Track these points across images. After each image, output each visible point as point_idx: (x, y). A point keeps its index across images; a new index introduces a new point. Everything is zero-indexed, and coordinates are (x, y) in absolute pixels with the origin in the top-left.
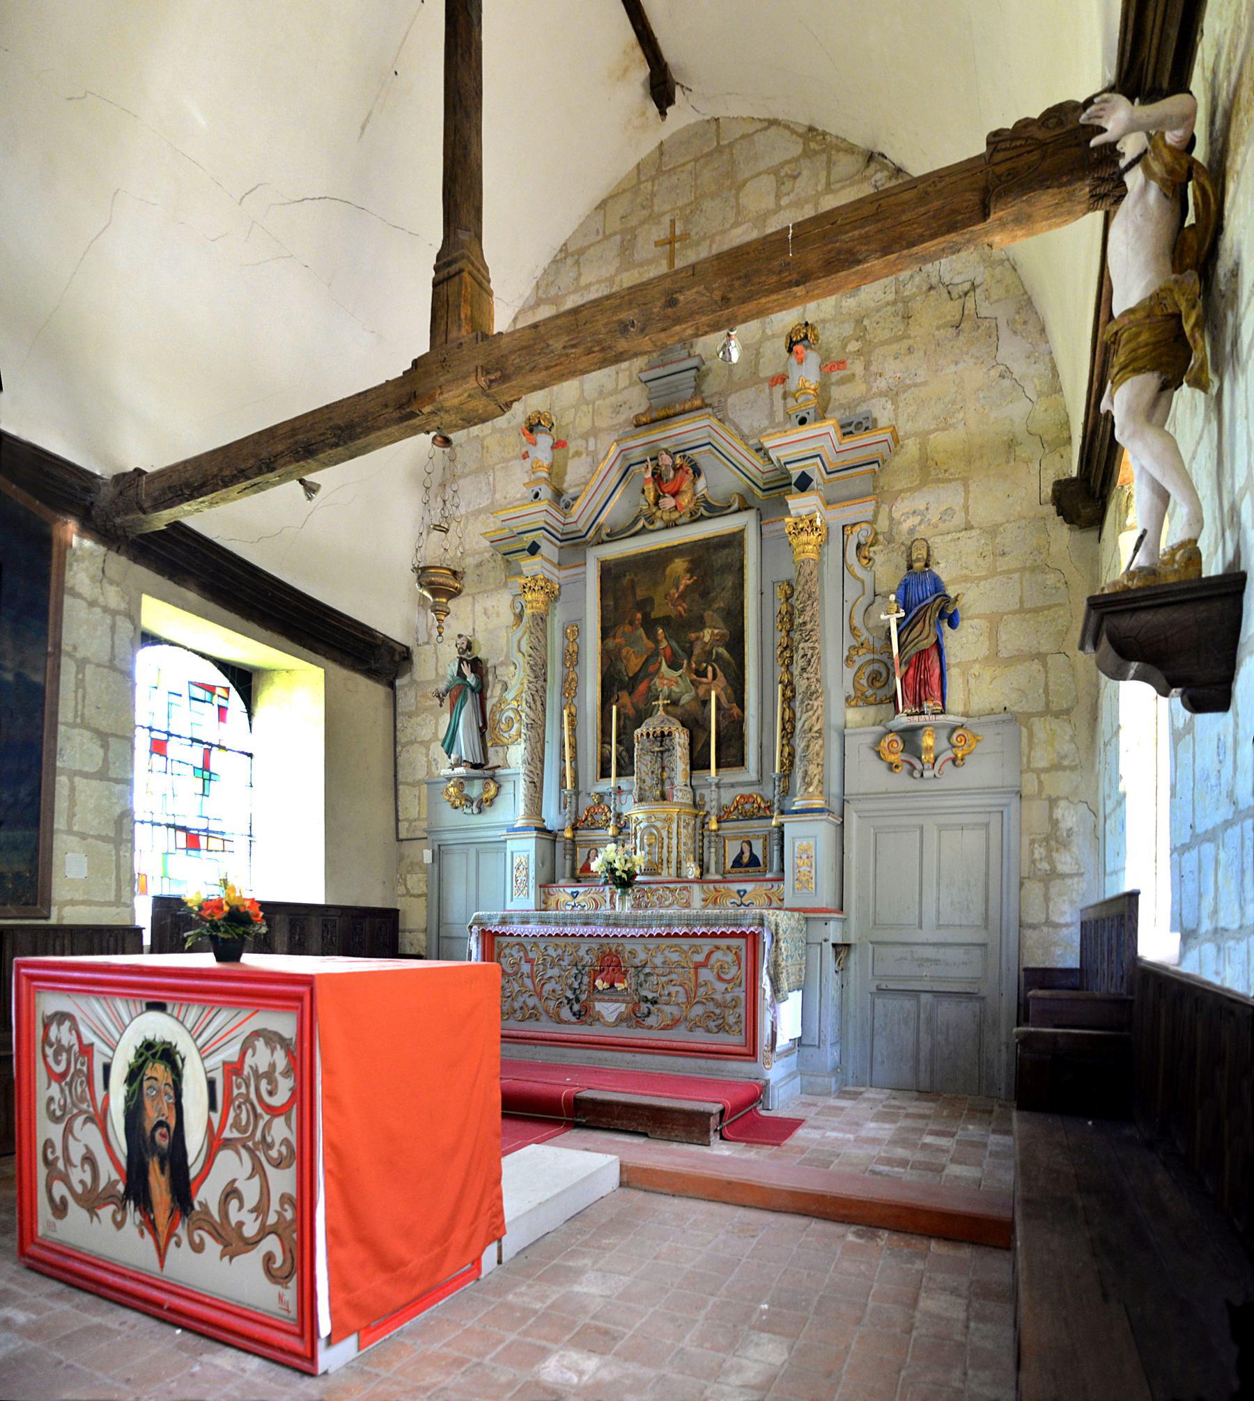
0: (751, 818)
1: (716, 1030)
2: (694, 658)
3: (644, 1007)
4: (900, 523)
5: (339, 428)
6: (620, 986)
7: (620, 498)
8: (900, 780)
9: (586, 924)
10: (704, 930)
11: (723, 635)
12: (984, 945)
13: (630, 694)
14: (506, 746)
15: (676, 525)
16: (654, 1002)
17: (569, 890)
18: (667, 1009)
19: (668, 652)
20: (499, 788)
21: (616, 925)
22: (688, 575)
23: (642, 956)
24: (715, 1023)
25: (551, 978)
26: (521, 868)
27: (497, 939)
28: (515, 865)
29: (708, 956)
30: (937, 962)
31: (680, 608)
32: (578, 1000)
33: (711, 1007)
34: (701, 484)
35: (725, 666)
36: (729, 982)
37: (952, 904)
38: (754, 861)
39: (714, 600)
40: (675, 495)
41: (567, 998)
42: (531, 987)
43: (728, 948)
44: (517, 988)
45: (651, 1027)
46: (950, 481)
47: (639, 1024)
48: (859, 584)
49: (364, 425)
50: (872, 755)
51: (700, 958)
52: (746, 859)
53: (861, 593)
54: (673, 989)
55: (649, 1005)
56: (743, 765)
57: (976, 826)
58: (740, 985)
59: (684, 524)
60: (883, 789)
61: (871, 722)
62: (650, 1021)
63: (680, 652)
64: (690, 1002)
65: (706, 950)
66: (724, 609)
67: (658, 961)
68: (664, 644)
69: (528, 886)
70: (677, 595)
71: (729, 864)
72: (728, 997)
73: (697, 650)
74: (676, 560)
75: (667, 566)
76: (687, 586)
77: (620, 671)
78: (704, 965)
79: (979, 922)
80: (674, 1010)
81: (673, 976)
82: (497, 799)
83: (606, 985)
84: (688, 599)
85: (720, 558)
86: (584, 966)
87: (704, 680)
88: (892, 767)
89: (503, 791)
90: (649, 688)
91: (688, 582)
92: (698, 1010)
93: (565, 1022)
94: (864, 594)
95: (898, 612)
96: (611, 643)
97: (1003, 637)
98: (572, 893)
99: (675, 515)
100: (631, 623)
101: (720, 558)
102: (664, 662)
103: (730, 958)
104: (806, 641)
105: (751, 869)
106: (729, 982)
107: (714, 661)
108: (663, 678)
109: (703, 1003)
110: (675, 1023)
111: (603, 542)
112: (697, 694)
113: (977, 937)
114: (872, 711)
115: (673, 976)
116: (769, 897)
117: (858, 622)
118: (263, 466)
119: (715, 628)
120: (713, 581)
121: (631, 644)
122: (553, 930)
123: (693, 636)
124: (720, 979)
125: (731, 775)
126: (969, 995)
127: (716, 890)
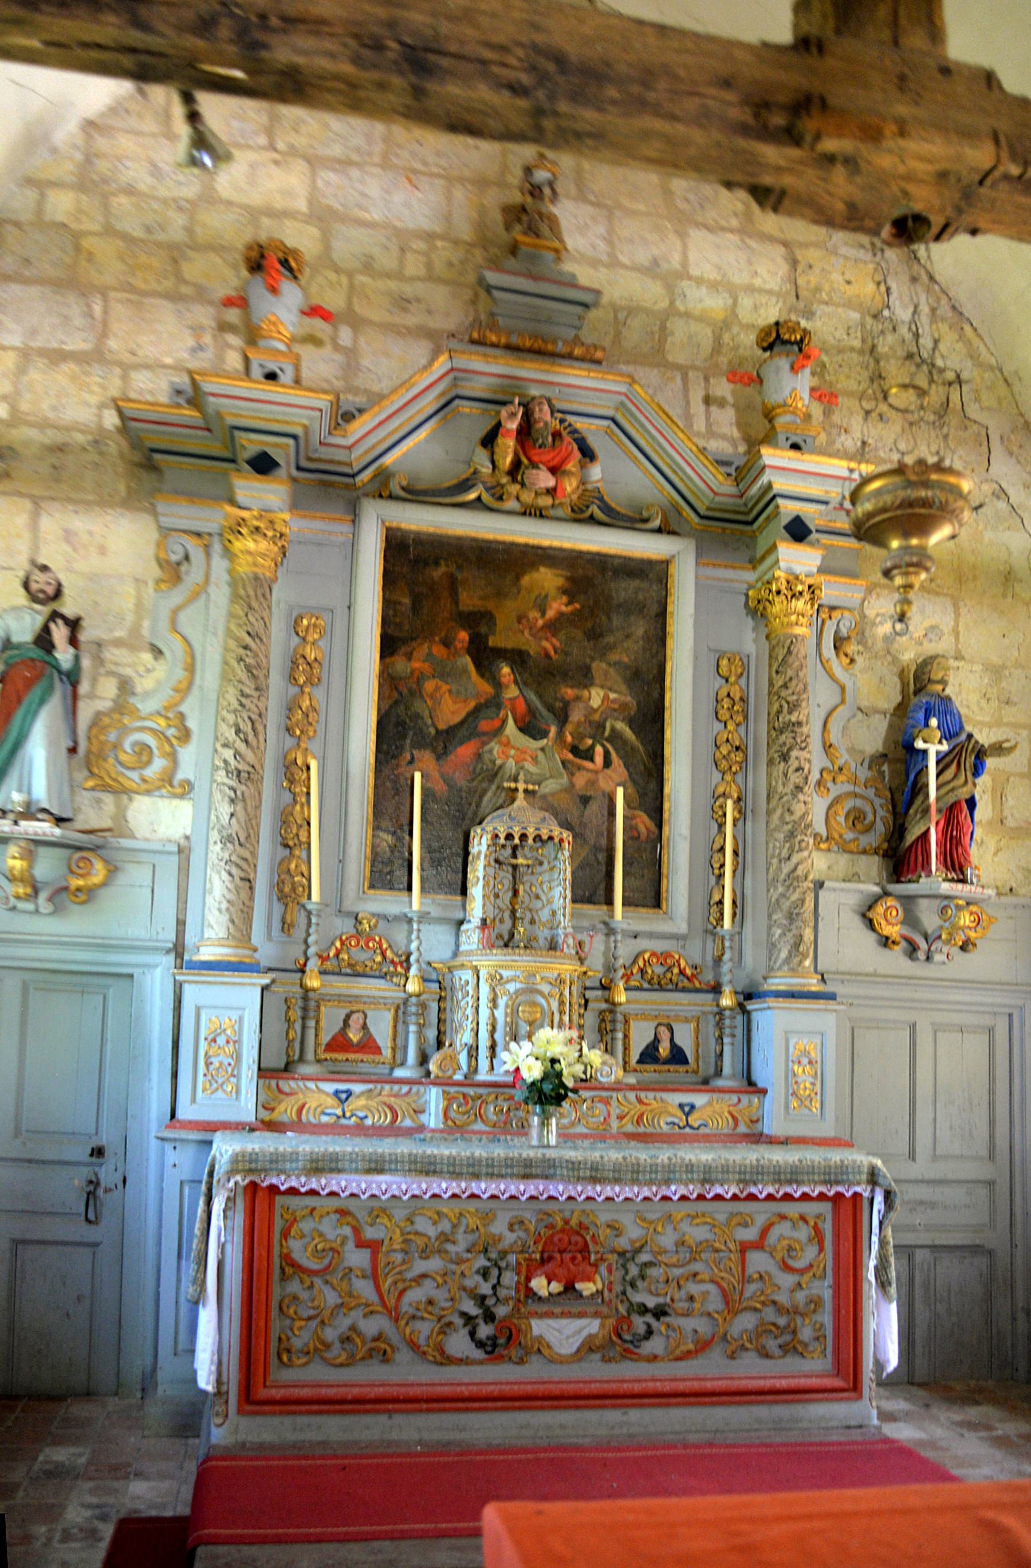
0: (661, 988)
1: (778, 1352)
2: (569, 728)
3: (639, 1323)
4: (874, 624)
5: (560, 60)
6: (587, 1288)
7: (427, 440)
8: (895, 960)
9: (526, 1177)
10: (770, 1189)
11: (624, 706)
12: (991, 1184)
13: (438, 758)
14: (121, 791)
15: (541, 516)
16: (660, 1313)
17: (330, 1087)
18: (687, 1324)
19: (522, 707)
20: (113, 870)
21: (594, 1180)
22: (565, 599)
23: (633, 1232)
24: (781, 1341)
25: (424, 1276)
26: (221, 1040)
27: (279, 1200)
28: (203, 1034)
29: (765, 1232)
30: (932, 1205)
31: (546, 644)
32: (489, 1317)
33: (770, 1314)
34: (596, 472)
35: (627, 754)
36: (802, 1272)
37: (951, 1128)
38: (678, 1056)
39: (611, 648)
40: (554, 470)
41: (464, 1314)
42: (372, 1296)
43: (803, 1218)
44: (331, 1298)
45: (655, 1358)
46: (937, 594)
47: (629, 1354)
48: (838, 689)
49: (636, 89)
50: (857, 922)
51: (750, 1234)
52: (664, 1050)
53: (838, 700)
54: (694, 1289)
55: (649, 1318)
56: (658, 905)
57: (975, 1029)
58: (824, 1276)
59: (558, 519)
60: (871, 970)
61: (841, 875)
62: (655, 1345)
63: (544, 712)
64: (732, 1304)
65: (760, 1221)
66: (627, 667)
67: (667, 1239)
68: (512, 692)
69: (238, 1077)
70: (540, 622)
71: (635, 1056)
72: (801, 1297)
73: (576, 715)
74: (542, 569)
75: (524, 573)
76: (561, 615)
77: (418, 716)
78: (758, 1245)
79: (985, 1153)
80: (703, 1326)
81: (697, 1267)
82: (103, 892)
83: (556, 1287)
84: (562, 635)
85: (624, 590)
86: (504, 1254)
87: (588, 764)
88: (886, 942)
89: (121, 879)
90: (479, 756)
91: (564, 609)
92: (746, 1322)
93: (460, 1361)
94: (843, 701)
95: (940, 742)
96: (400, 665)
97: (1010, 802)
98: (337, 1093)
99: (546, 501)
100: (447, 643)
101: (624, 590)
102: (511, 721)
103: (803, 1233)
104: (802, 749)
105: (672, 1068)
106: (802, 1272)
107: (607, 740)
108: (507, 744)
109: (756, 1310)
110: (703, 1346)
111: (391, 497)
112: (572, 785)
113: (985, 1171)
114: (843, 859)
115: (697, 1267)
116: (733, 1117)
117: (834, 737)
118: (225, 22)
119: (610, 689)
120: (609, 618)
121: (443, 673)
122: (445, 1186)
123: (569, 692)
124: (786, 1268)
125: (645, 920)
126: (975, 1249)
127: (640, 1101)
